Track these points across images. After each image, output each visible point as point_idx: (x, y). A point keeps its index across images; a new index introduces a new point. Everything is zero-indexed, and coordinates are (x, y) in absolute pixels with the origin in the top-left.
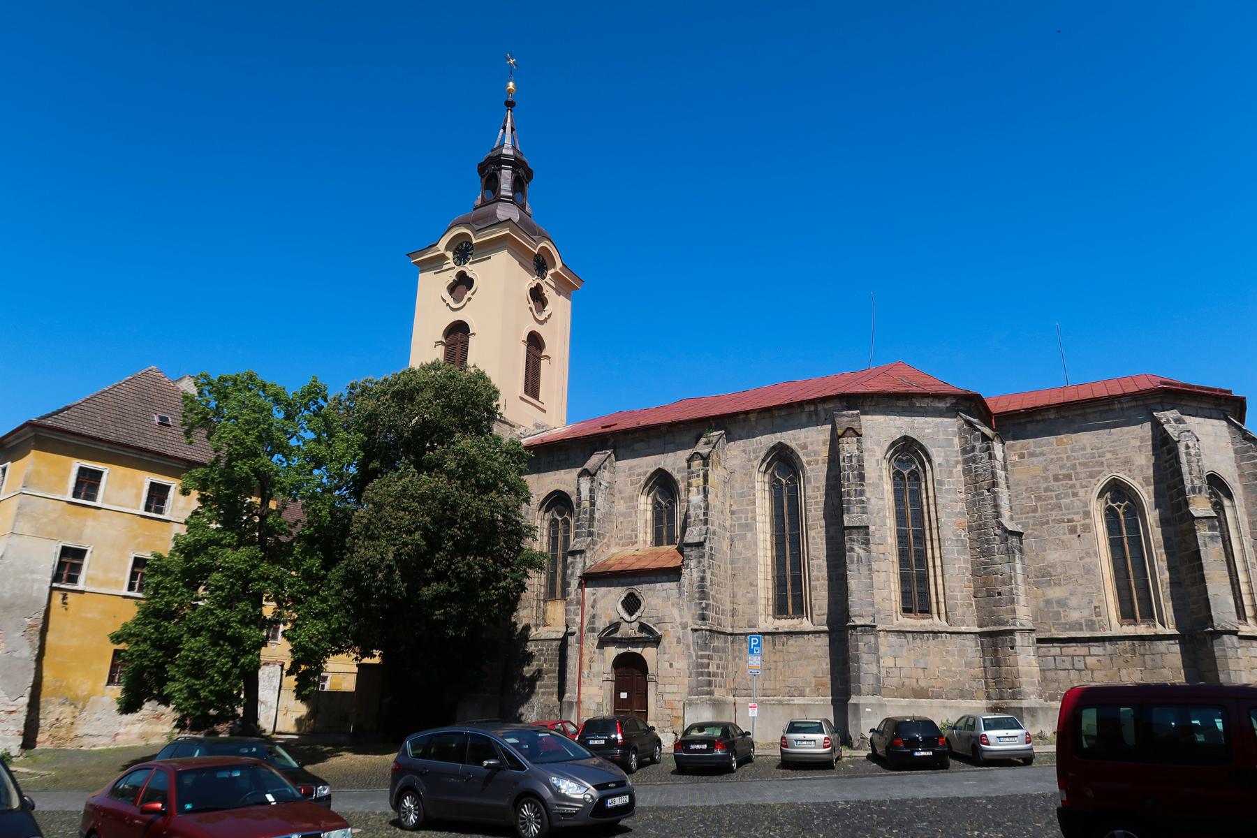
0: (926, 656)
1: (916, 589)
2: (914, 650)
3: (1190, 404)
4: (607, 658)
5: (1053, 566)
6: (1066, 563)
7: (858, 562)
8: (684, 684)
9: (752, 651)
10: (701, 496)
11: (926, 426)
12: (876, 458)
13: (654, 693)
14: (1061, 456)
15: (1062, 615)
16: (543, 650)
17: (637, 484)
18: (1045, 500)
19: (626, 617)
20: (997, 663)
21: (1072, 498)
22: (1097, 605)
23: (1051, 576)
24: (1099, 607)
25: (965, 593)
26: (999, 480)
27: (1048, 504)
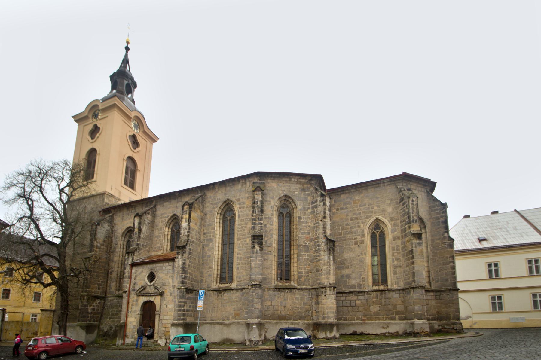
0: (286, 300)
1: (284, 269)
2: (280, 297)
4: (139, 304)
5: (346, 260)
6: (352, 258)
7: (256, 253)
8: (171, 315)
10: (187, 223)
11: (295, 190)
12: (271, 205)
13: (158, 320)
14: (355, 209)
15: (348, 282)
16: (119, 301)
17: (164, 222)
18: (345, 230)
19: (149, 283)
20: (317, 303)
21: (357, 228)
22: (363, 277)
23: (345, 264)
24: (364, 278)
25: (306, 271)
26: (327, 216)
27: (346, 232)
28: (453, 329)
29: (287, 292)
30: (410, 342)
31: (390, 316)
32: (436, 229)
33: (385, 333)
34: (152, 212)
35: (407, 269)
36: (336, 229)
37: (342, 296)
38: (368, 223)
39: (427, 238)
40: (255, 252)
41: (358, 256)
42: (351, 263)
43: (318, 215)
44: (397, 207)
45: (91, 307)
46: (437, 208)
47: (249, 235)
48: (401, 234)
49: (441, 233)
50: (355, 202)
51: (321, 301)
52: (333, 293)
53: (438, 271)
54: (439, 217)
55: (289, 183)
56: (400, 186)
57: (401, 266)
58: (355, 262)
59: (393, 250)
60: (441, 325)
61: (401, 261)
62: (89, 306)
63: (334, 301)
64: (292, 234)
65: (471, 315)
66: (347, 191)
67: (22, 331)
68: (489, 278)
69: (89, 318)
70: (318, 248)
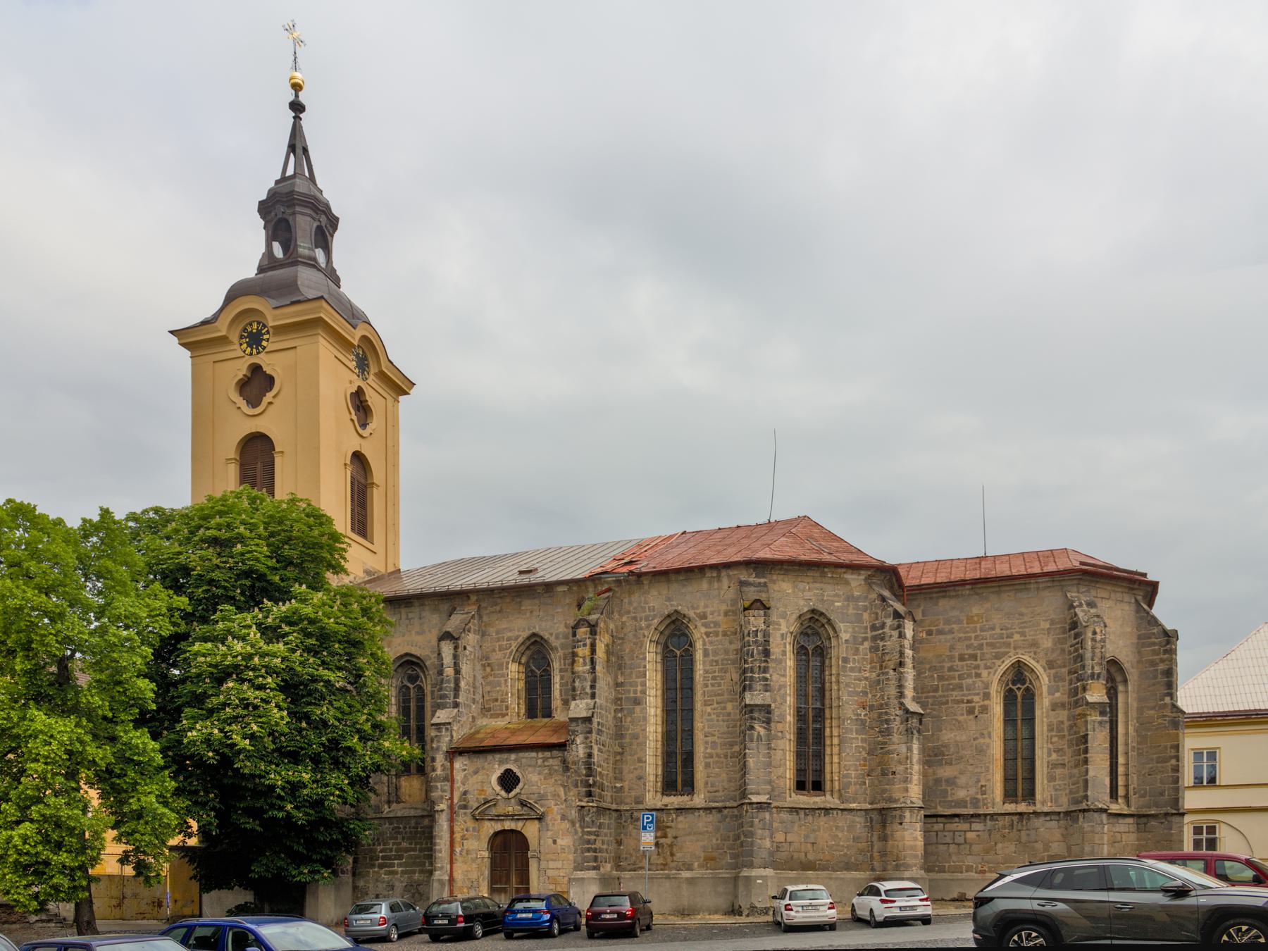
1: (811, 768)
3: (1104, 587)
5: (946, 746)
7: (758, 741)
9: (645, 828)
11: (836, 599)
12: (781, 632)
16: (400, 828)
18: (947, 680)
20: (884, 838)
21: (974, 679)
22: (983, 784)
24: (985, 786)
27: (949, 684)
35: (1075, 771)
37: (937, 823)
38: (999, 670)
40: (755, 737)
41: (974, 739)
42: (958, 753)
43: (887, 658)
44: (1064, 638)
46: (1153, 640)
47: (731, 695)
48: (1069, 697)
50: (970, 620)
51: (892, 835)
54: (1157, 661)
55: (821, 583)
57: (1064, 764)
58: (967, 752)
59: (1051, 730)
61: (1065, 755)
62: (189, 830)
63: (919, 835)
64: (827, 694)
66: (953, 594)
70: (886, 726)
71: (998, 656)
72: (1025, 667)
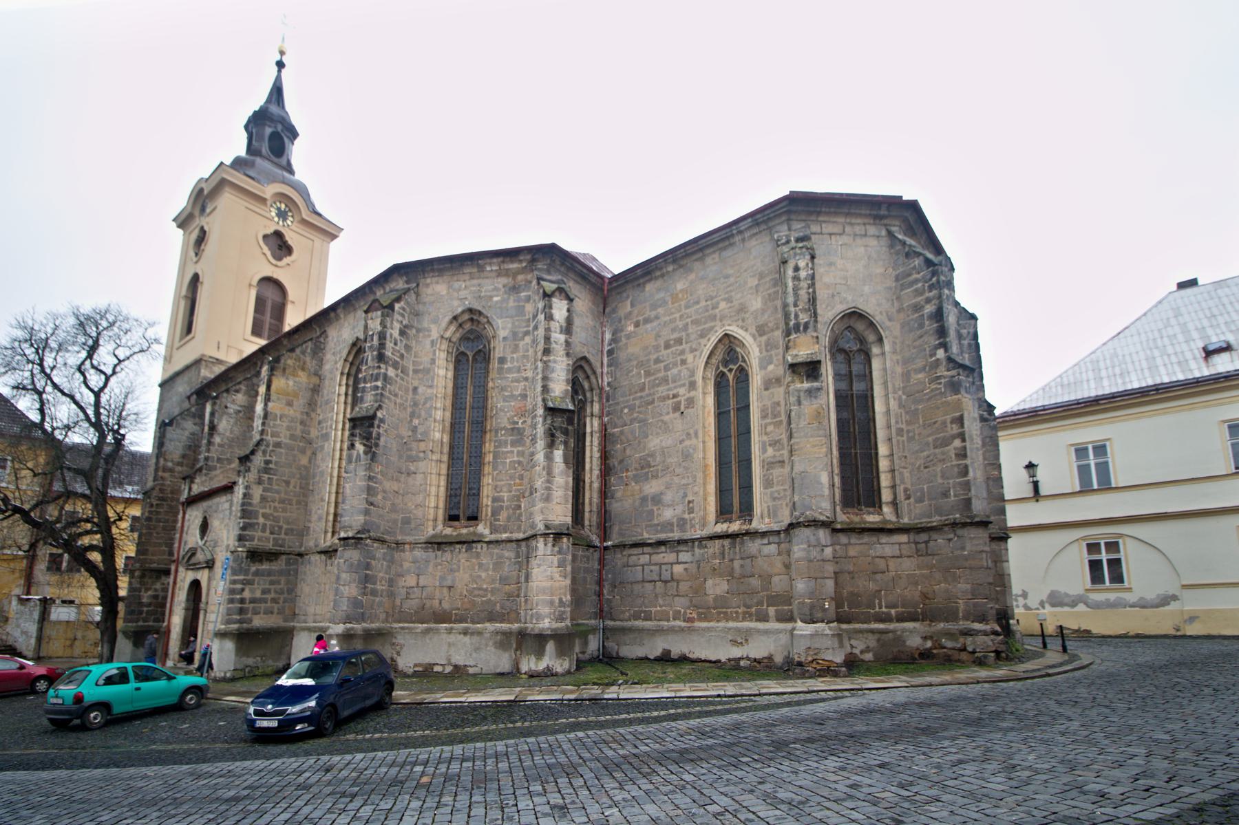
3: (835, 220)
5: (652, 455)
11: (495, 293)
18: (653, 374)
22: (691, 499)
23: (650, 466)
26: (554, 345)
28: (964, 649)
29: (460, 552)
30: (719, 696)
31: (753, 610)
32: (915, 341)
33: (740, 659)
34: (247, 386)
36: (633, 376)
37: (643, 554)
39: (885, 370)
45: (150, 593)
46: (915, 276)
49: (928, 349)
50: (675, 298)
52: (552, 551)
53: (922, 468)
55: (478, 278)
56: (782, 231)
57: (783, 462)
60: (931, 638)
61: (783, 449)
65: (1177, 594)
66: (658, 273)
67: (75, 639)
68: (1234, 471)
69: (144, 615)
71: (703, 335)
72: (737, 342)
